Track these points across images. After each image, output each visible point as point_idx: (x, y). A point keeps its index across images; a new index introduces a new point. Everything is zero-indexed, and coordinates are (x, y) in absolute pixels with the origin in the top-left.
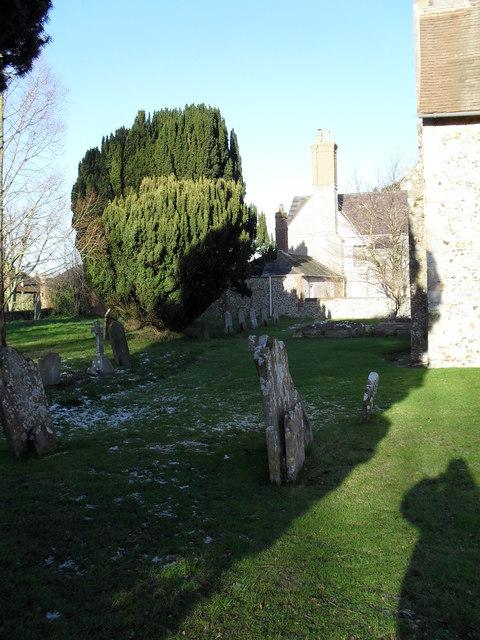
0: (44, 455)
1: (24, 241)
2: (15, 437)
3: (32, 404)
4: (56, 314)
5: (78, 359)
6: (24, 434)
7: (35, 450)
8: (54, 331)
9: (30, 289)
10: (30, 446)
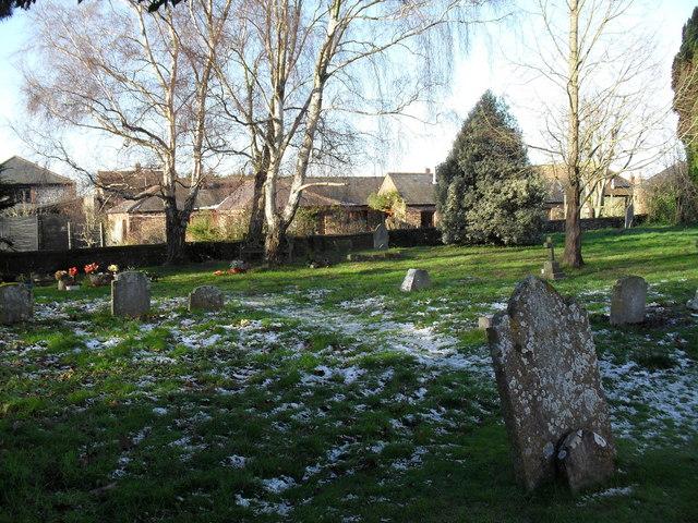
0: (582, 491)
1: (615, 133)
2: (528, 452)
3: (570, 386)
4: (652, 221)
5: (676, 283)
6: (550, 445)
7: (566, 480)
8: (647, 242)
9: (622, 192)
10: (557, 469)
